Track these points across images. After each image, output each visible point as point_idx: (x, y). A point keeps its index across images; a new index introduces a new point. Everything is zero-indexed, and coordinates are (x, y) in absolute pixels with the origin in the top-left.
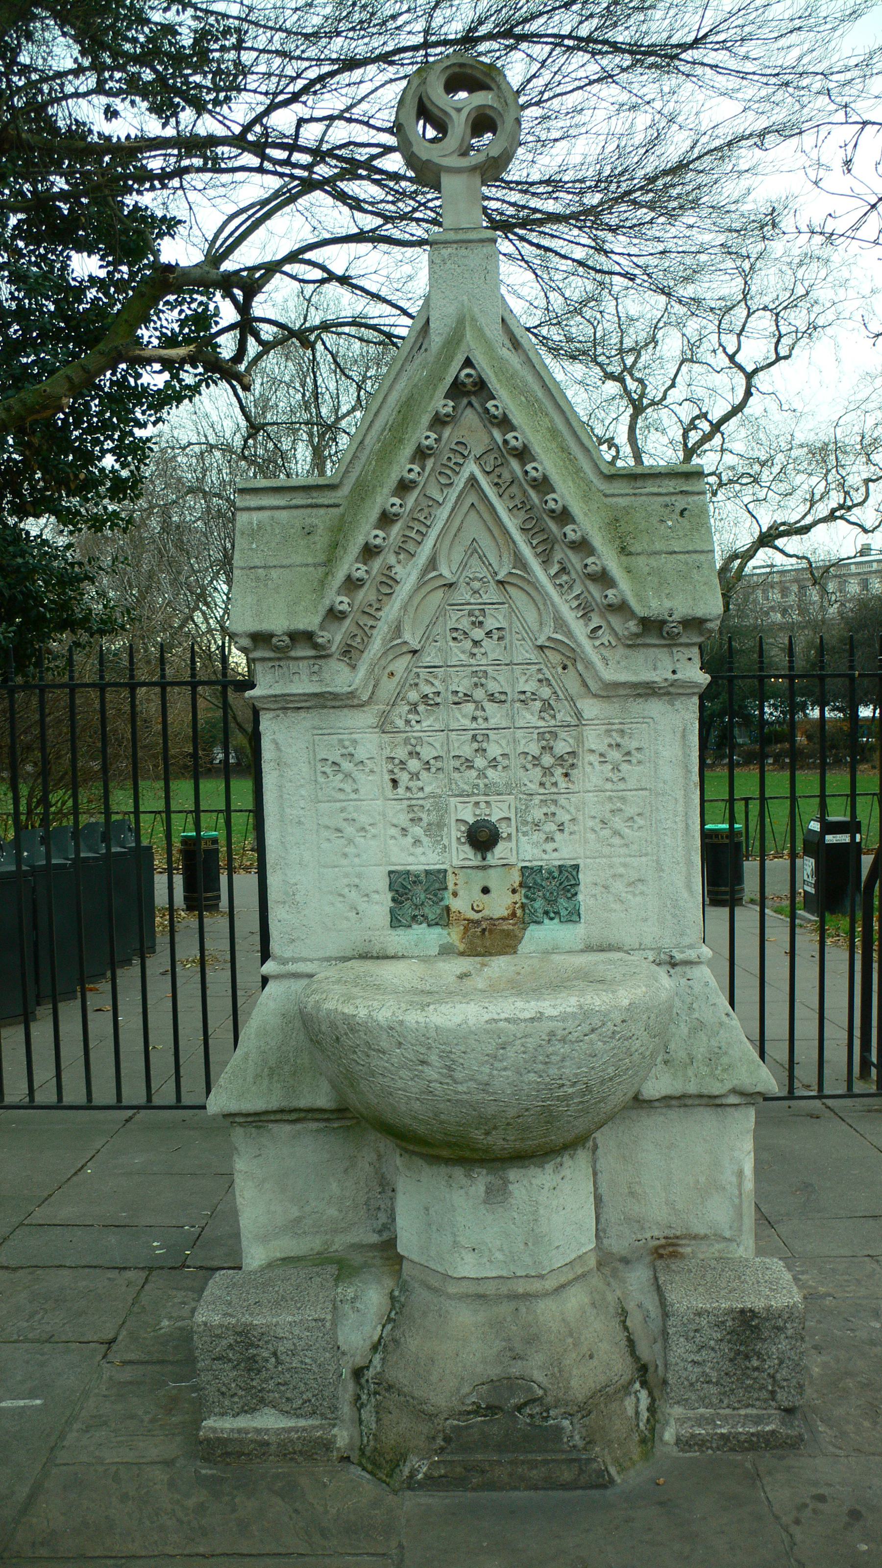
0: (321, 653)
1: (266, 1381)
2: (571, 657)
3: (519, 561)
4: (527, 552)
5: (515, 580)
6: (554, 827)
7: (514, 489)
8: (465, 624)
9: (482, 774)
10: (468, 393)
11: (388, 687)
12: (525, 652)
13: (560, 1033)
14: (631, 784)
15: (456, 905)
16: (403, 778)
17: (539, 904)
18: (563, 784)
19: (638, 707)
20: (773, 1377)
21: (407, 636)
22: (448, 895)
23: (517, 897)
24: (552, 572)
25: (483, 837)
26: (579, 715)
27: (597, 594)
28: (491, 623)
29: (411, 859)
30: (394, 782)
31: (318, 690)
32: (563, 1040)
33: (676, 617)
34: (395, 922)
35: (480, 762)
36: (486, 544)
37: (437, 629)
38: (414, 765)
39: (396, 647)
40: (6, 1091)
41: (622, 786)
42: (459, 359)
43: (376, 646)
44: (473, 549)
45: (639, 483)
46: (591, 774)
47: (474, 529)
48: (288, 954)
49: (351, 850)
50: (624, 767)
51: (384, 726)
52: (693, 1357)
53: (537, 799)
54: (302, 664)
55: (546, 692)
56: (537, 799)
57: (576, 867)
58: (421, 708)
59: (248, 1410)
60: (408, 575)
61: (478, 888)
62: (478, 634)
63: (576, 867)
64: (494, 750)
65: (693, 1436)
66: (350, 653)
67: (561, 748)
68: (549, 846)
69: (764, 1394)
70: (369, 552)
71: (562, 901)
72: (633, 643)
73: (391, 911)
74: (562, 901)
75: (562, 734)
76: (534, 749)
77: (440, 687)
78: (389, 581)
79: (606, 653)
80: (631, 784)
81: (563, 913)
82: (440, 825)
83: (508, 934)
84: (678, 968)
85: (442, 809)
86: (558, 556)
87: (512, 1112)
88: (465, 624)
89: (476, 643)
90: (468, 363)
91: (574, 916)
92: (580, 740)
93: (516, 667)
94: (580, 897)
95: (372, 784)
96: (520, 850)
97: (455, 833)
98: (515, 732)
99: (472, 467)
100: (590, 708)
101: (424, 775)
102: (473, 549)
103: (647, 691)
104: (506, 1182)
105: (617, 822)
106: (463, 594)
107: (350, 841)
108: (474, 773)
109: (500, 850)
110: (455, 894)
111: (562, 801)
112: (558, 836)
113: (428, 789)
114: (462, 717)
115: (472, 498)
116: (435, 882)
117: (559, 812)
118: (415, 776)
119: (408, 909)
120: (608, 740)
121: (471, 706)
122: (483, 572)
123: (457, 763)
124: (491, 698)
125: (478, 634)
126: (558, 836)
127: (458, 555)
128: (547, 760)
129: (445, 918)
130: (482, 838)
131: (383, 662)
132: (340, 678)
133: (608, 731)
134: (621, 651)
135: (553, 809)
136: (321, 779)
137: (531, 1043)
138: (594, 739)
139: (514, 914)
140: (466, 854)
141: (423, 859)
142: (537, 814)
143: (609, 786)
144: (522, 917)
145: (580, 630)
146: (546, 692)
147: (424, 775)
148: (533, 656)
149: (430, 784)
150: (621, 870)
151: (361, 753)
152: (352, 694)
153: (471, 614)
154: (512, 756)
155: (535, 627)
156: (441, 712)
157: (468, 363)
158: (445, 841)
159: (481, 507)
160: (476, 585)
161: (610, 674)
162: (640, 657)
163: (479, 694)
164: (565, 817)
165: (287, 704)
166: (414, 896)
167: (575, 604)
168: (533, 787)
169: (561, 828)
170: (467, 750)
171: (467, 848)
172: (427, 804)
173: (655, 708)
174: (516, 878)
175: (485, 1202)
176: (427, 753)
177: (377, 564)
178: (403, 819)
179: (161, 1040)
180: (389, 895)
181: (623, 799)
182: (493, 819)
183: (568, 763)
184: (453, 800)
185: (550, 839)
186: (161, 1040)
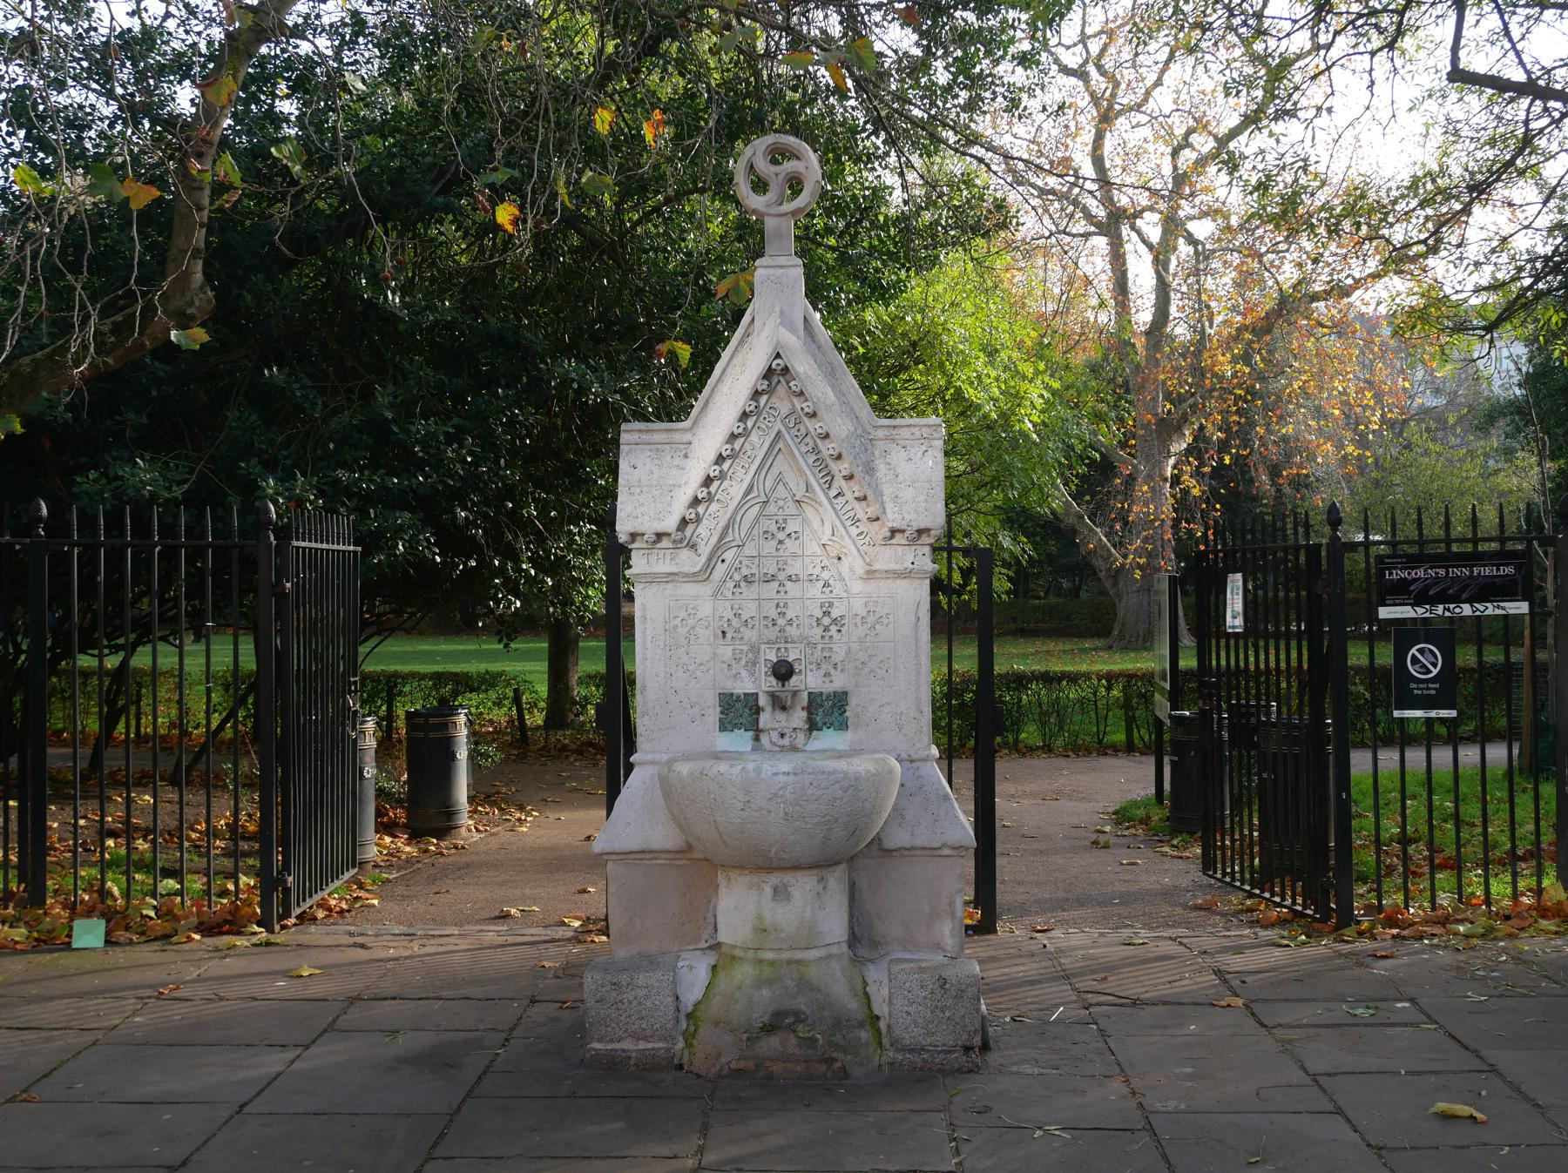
7: (808, 439)
8: (773, 528)
31: (675, 570)
34: (724, 727)
35: (781, 622)
40: (999, 848)
85: (754, 649)
86: (835, 484)
88: (773, 528)
89: (781, 542)
91: (843, 726)
97: (763, 669)
109: (794, 680)
124: (790, 578)
170: (773, 613)
171: (772, 679)
179: (1223, 654)
180: (718, 709)
186: (1223, 654)
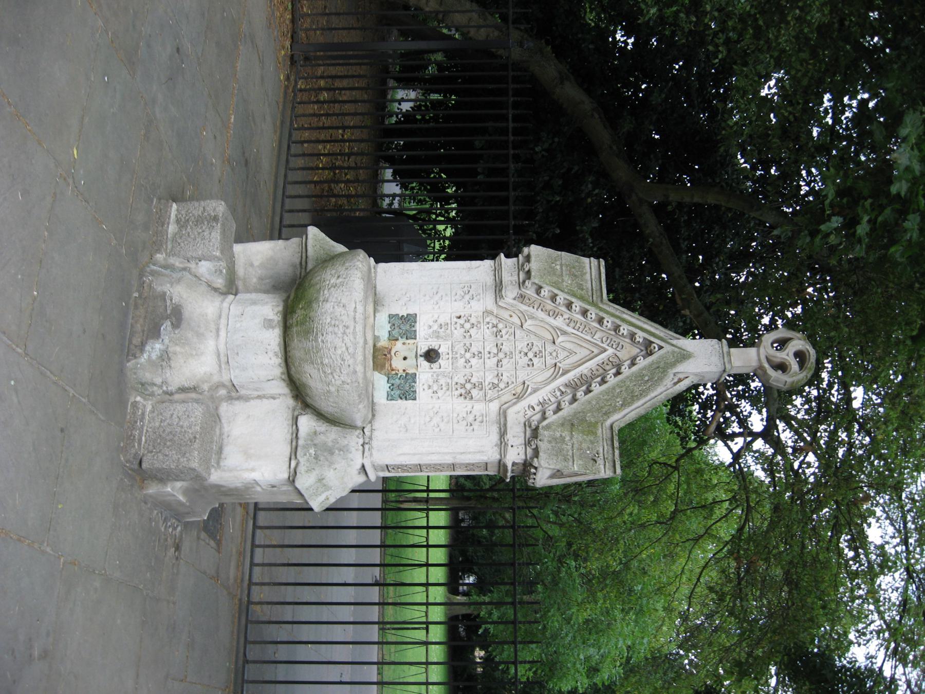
0: (521, 284)
1: (191, 228)
2: (519, 397)
3: (566, 372)
4: (570, 376)
5: (557, 370)
6: (435, 389)
7: (601, 371)
8: (535, 349)
9: (462, 356)
10: (647, 349)
11: (505, 314)
12: (522, 375)
13: (347, 331)
14: (456, 426)
15: (399, 344)
16: (461, 321)
17: (397, 382)
18: (458, 393)
19: (495, 430)
20: (160, 451)
21: (529, 322)
22: (404, 340)
23: (401, 371)
24: (561, 388)
25: (432, 354)
26: (491, 401)
27: (550, 408)
28: (535, 360)
29: (422, 324)
30: (460, 317)
32: (344, 333)
33: (539, 443)
35: (468, 355)
36: (574, 359)
37: (533, 337)
38: (467, 326)
39: (523, 317)
41: (455, 421)
42: (662, 344)
43: (523, 308)
44: (572, 353)
45: (609, 443)
46: (461, 406)
47: (582, 353)
48: (379, 270)
49: (427, 298)
50: (465, 423)
51: (487, 313)
52: (176, 413)
53: (450, 381)
54: (516, 278)
55: (502, 385)
56: (450, 381)
57: (415, 399)
58: (495, 329)
59: (178, 221)
60: (559, 322)
61: (406, 354)
62: (531, 355)
63: (415, 399)
64: (474, 361)
65: (138, 409)
66: (522, 298)
67: (474, 392)
68: (426, 387)
69: (151, 448)
70: (569, 306)
71: (398, 392)
72: (527, 424)
73: (397, 315)
74: (398, 392)
75: (481, 393)
76: (474, 380)
77: (505, 337)
78: (555, 315)
79: (522, 414)
80: (456, 426)
81: (392, 393)
82: (438, 337)
83: (383, 366)
84: (361, 448)
87: (312, 314)
88: (535, 349)
89: (526, 354)
90: (661, 348)
91: (390, 398)
92: (478, 401)
93: (515, 371)
94: (400, 401)
95: (459, 307)
96: (425, 372)
97: (434, 344)
98: (482, 371)
99: (610, 351)
100: (494, 406)
101: (463, 330)
102: (572, 353)
103: (503, 433)
104: (273, 328)
105: (436, 420)
106: (550, 348)
107: (431, 298)
108: (463, 352)
110: (404, 344)
111: (449, 393)
112: (431, 391)
113: (455, 331)
114: (490, 347)
115: (596, 351)
116: (411, 335)
117: (443, 391)
118: (462, 326)
119: (397, 322)
120: (478, 414)
121: (496, 351)
122: (561, 357)
123: (468, 345)
124: (499, 361)
125: (531, 355)
126: (431, 391)
127: (569, 346)
128: (468, 386)
129: (393, 339)
130: (431, 356)
131: (517, 312)
132: (510, 293)
133: (483, 415)
134: (523, 420)
135: (445, 389)
136: (462, 286)
137: (344, 318)
138: (479, 408)
139: (393, 370)
140: (423, 349)
141: (422, 329)
142: (442, 381)
143: (455, 415)
144: (391, 375)
145: (533, 400)
146: (502, 385)
147: (463, 330)
148: (520, 380)
149: (458, 333)
150: (412, 421)
151: (473, 303)
152: (501, 297)
153: (541, 352)
154: (471, 370)
155: (534, 381)
156: (493, 338)
157: (661, 348)
158: (430, 340)
159: (592, 355)
160: (554, 354)
161: (511, 413)
162: (520, 429)
163: (501, 355)
164: (440, 393)
165: (497, 272)
166: (405, 325)
167: (546, 398)
168: (455, 380)
169: (435, 392)
170: (474, 349)
172: (449, 331)
173: (495, 437)
174: (411, 371)
175: (265, 319)
176: (473, 332)
177: (564, 309)
178: (441, 321)
181: (448, 422)
182: (440, 361)
183: (467, 396)
184: (450, 343)
185: (430, 387)
